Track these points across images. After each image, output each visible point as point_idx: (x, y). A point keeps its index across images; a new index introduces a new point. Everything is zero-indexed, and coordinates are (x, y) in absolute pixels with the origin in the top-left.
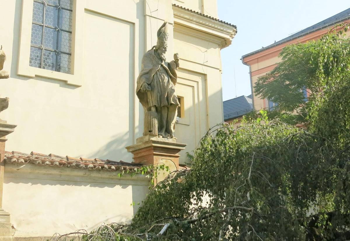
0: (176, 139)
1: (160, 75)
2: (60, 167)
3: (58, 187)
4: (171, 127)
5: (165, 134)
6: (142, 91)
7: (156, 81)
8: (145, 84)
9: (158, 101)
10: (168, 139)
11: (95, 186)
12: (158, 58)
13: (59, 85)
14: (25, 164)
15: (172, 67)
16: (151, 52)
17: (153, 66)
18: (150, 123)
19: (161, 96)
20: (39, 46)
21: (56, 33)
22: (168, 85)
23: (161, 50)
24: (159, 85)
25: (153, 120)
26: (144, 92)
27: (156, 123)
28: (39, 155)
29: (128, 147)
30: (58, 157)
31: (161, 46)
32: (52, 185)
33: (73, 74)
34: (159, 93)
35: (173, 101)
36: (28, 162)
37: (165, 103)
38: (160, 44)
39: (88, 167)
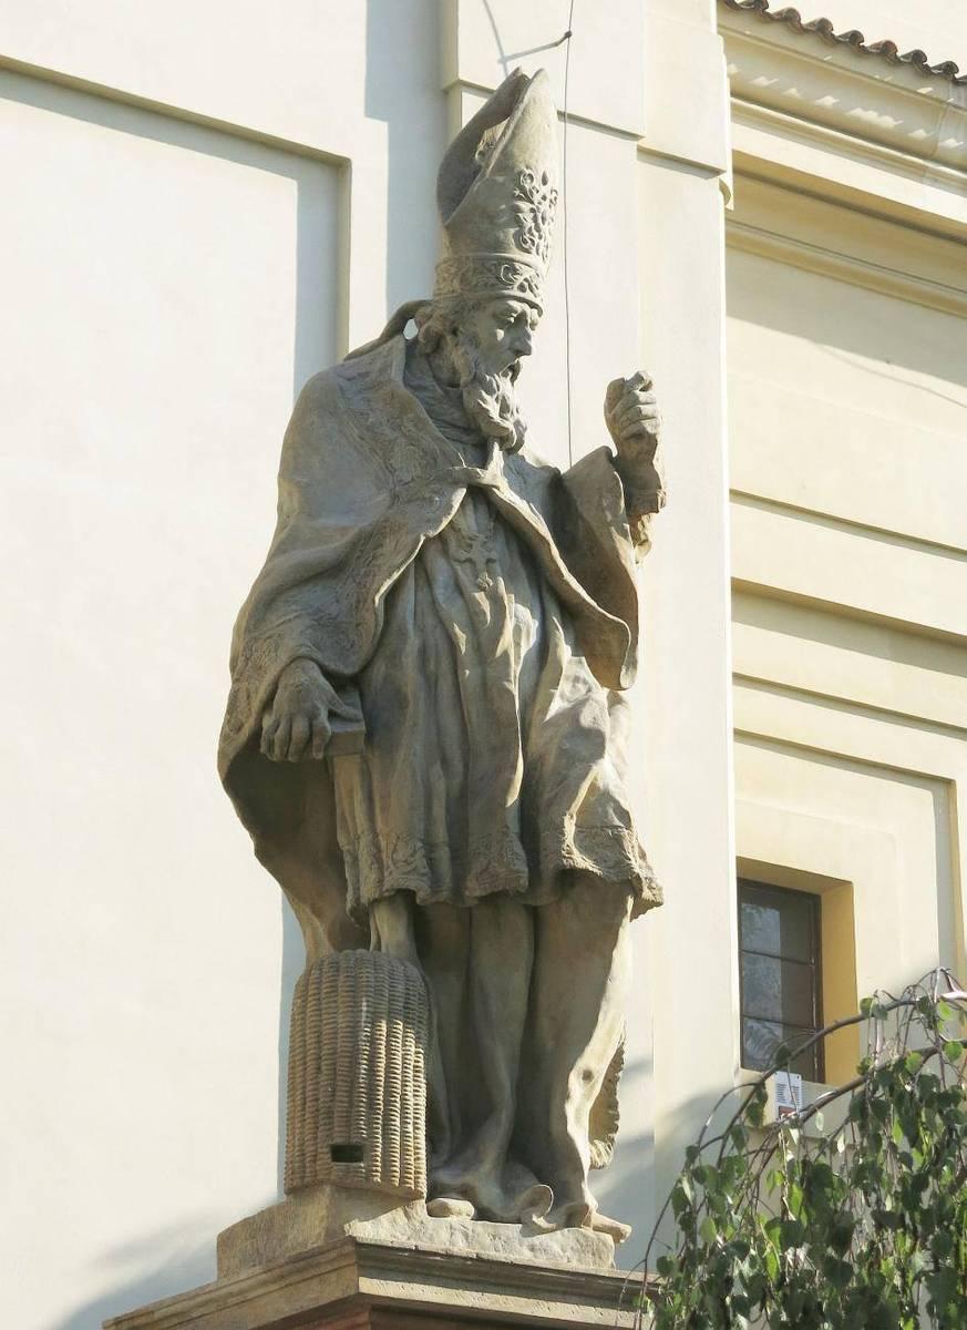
0: (617, 1234)
1: (459, 589)
4: (570, 1109)
5: (508, 1190)
6: (271, 745)
7: (413, 643)
9: (430, 847)
10: (531, 1230)
12: (436, 420)
15: (587, 511)
16: (378, 365)
17: (395, 497)
18: (343, 1062)
19: (461, 803)
22: (537, 684)
23: (474, 341)
24: (445, 686)
25: (373, 1041)
27: (407, 1067)
31: (478, 306)
34: (445, 762)
35: (586, 850)
37: (502, 871)
38: (464, 280)
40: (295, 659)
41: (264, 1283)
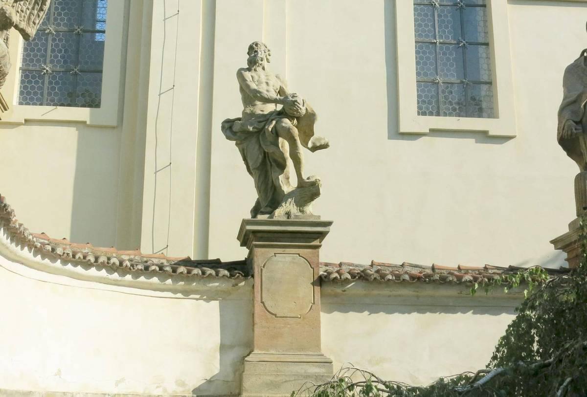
2: (413, 283)
3: (415, 317)
8: (569, 123)
11: (483, 312)
13: (474, 140)
14: (353, 281)
20: (432, 78)
21: (461, 50)
26: (569, 138)
28: (383, 265)
29: (553, 240)
30: (416, 266)
32: (403, 313)
33: (497, 117)
36: (357, 277)
39: (463, 280)
40: (567, 120)
41: (573, 233)
